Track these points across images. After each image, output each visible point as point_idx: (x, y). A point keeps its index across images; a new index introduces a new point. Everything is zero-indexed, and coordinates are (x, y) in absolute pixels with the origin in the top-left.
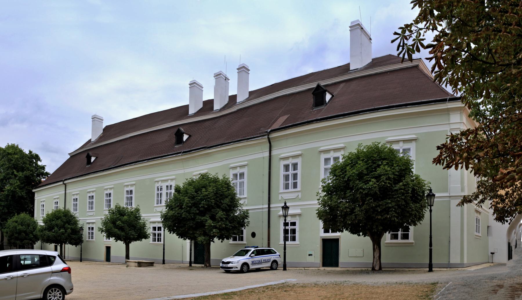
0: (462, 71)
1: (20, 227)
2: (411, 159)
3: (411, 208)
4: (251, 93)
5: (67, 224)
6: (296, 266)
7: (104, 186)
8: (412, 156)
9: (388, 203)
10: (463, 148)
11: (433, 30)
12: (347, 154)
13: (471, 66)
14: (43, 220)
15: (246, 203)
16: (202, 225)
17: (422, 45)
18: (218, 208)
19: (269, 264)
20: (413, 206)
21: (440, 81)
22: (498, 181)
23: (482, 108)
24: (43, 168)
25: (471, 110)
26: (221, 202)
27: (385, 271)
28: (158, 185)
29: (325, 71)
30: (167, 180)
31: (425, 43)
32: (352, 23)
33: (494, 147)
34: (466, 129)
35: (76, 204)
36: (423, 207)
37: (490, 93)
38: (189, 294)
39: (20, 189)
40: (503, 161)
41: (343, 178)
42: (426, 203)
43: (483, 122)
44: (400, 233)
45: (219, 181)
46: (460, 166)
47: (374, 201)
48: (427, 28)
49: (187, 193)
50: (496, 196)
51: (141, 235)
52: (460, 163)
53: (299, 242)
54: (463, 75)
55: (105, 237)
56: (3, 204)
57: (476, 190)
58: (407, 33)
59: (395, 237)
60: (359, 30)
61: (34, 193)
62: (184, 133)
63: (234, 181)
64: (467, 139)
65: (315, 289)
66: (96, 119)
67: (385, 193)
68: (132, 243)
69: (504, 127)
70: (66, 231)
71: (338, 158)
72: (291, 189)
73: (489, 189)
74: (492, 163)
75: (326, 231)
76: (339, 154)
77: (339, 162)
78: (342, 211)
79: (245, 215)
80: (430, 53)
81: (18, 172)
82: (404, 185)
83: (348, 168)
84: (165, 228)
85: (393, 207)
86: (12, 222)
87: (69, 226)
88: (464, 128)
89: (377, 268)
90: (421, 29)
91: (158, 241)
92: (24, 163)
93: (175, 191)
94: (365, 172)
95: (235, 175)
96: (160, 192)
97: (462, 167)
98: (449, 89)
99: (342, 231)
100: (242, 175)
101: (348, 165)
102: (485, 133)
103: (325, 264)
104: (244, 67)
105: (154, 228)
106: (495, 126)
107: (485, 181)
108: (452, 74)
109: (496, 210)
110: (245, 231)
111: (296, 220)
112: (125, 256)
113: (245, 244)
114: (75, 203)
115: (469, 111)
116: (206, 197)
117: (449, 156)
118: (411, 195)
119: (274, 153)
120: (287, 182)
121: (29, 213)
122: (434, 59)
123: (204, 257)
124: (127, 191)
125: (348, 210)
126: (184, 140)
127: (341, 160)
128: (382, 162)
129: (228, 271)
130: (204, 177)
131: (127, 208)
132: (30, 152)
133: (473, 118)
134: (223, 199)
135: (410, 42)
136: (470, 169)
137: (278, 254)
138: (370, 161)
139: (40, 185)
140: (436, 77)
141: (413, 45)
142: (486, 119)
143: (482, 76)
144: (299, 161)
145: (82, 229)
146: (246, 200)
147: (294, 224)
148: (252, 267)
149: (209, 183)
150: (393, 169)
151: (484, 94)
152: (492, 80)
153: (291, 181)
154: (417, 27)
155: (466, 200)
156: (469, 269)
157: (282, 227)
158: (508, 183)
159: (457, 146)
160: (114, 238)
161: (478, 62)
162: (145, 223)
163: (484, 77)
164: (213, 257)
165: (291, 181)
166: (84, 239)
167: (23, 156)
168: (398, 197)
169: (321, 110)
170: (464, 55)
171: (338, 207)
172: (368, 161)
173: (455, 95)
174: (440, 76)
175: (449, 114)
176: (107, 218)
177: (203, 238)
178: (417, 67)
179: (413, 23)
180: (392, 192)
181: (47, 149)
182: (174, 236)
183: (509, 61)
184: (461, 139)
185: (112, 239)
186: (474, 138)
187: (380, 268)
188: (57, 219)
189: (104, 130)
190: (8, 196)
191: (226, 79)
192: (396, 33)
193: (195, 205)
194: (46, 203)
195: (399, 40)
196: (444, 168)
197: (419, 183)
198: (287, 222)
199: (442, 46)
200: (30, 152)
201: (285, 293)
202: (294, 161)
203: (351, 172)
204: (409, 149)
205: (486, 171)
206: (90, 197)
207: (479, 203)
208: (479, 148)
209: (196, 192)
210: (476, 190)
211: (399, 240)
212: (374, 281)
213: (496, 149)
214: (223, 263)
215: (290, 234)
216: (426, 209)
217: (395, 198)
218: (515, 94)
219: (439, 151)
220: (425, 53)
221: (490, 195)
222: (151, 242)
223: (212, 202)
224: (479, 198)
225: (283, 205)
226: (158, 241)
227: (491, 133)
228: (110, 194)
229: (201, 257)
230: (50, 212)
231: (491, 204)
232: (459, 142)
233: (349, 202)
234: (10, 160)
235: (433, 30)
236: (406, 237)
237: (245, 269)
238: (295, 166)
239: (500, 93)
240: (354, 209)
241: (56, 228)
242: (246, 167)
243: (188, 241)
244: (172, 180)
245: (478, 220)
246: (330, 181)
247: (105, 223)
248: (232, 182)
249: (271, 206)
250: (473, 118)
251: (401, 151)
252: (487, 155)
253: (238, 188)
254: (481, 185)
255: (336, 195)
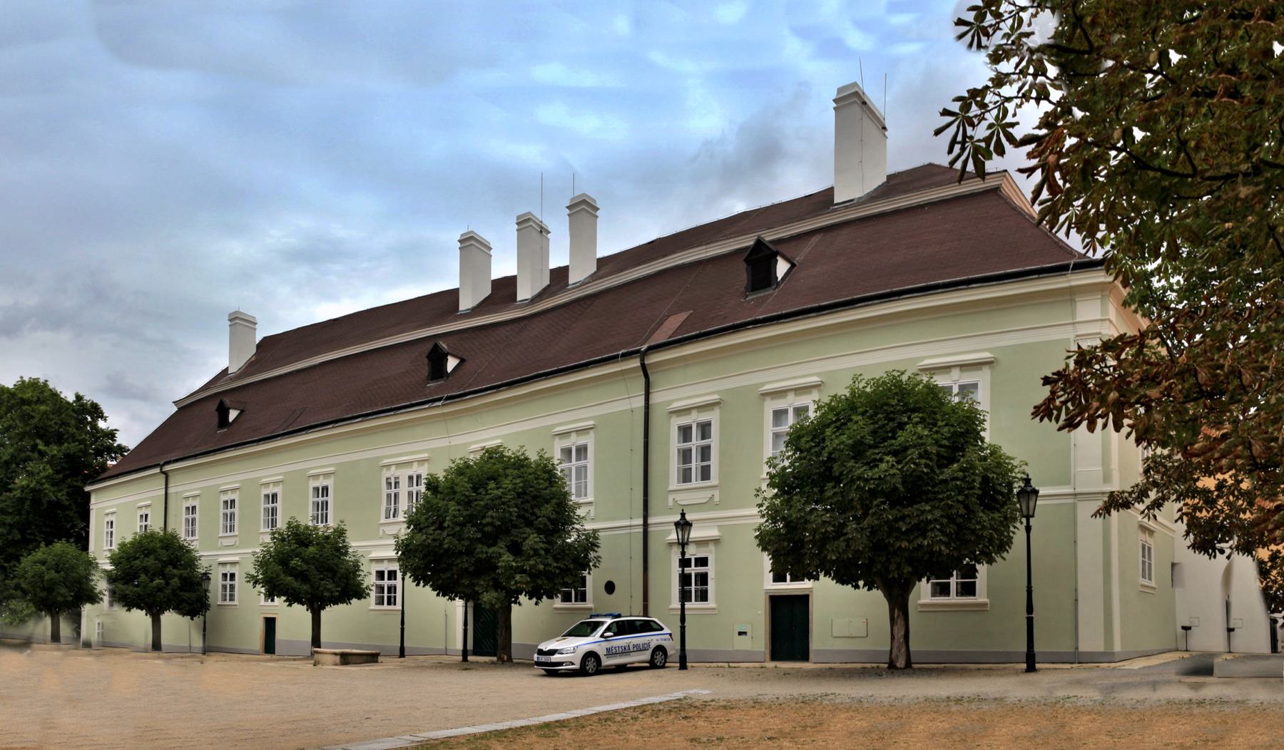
0: (1109, 197)
1: (53, 574)
2: (980, 408)
3: (979, 523)
4: (602, 262)
5: (170, 567)
6: (708, 658)
7: (260, 478)
8: (983, 400)
9: (924, 512)
10: (1108, 379)
11: (1038, 100)
12: (826, 400)
13: (1133, 185)
14: (111, 558)
15: (592, 514)
16: (487, 566)
17: (1011, 139)
18: (527, 526)
19: (646, 656)
20: (985, 518)
21: (1053, 224)
22: (1197, 455)
23: (1156, 283)
24: (111, 435)
25: (1128, 289)
26: (534, 514)
27: (919, 669)
28: (388, 475)
29: (773, 206)
30: (409, 464)
31: (1018, 133)
32: (840, 90)
33: (1187, 376)
34: (1116, 335)
35: (193, 520)
36: (1008, 520)
37: (1178, 248)
38: (462, 726)
39: (52, 485)
40: (1211, 409)
41: (818, 454)
42: (1017, 510)
43: (1159, 316)
44: (953, 581)
45: (529, 466)
46: (1100, 422)
47: (892, 506)
48: (1024, 96)
49: (455, 493)
50: (1194, 492)
51: (349, 589)
52: (1100, 416)
53: (717, 602)
54: (1111, 207)
55: (262, 596)
56: (9, 520)
57: (1140, 479)
58: (975, 110)
59: (943, 590)
60: (857, 109)
61: (88, 495)
62: (448, 354)
63: (564, 465)
64: (1117, 358)
65: (756, 712)
66: (240, 322)
67: (916, 489)
68: (328, 608)
69: (1213, 328)
70: (167, 584)
71: (806, 409)
72: (696, 482)
73: (1175, 476)
74: (1180, 413)
75: (779, 578)
76: (807, 400)
77: (807, 417)
78: (814, 532)
79: (590, 542)
80: (1030, 155)
81: (47, 444)
82: (962, 470)
83: (828, 432)
84: (404, 574)
85: (936, 520)
86: (32, 562)
87: (175, 571)
88: (1112, 333)
89: (900, 662)
90: (1009, 99)
91: (389, 603)
92: (64, 424)
93: (428, 489)
94: (869, 440)
95: (567, 452)
96: (393, 491)
97: (1105, 426)
98: (1075, 241)
99: (817, 578)
100: (582, 451)
101: (828, 426)
102: (1163, 343)
103: (777, 653)
104: (584, 202)
105: (380, 575)
106: (1191, 325)
107: (1165, 457)
108: (1084, 206)
109: (1193, 525)
110: (589, 580)
111: (709, 552)
112: (310, 639)
113: (590, 609)
114: (190, 516)
115: (1125, 292)
116: (497, 502)
117: (1072, 400)
118: (980, 492)
119: (656, 398)
120: (687, 466)
121: (76, 542)
122: (1039, 171)
123: (495, 640)
124: (316, 489)
125: (830, 529)
126: (449, 370)
127: (812, 415)
128: (909, 418)
129: (553, 671)
130: (492, 455)
131: (316, 528)
132: (79, 398)
133: (1133, 307)
134: (538, 506)
135: (981, 132)
136: (1126, 430)
137: (666, 630)
138: (880, 416)
139: (103, 476)
140: (1043, 214)
141: (987, 140)
142: (1168, 309)
143: (1160, 207)
144: (713, 417)
145: (206, 577)
146: (592, 509)
147: (703, 562)
148: (606, 662)
149: (505, 469)
150: (937, 432)
151: (1163, 249)
152: (1186, 216)
153: (695, 464)
154: (999, 95)
155: (1116, 502)
156: (1127, 665)
157: (676, 570)
158: (1224, 462)
159: (1093, 375)
160: (284, 598)
161: (1151, 174)
162: (357, 561)
163: (1163, 209)
164: (517, 637)
165: (696, 464)
166: (211, 601)
167: (60, 408)
168: (949, 497)
169: (765, 298)
170: (1115, 158)
171: (806, 522)
172: (876, 414)
173: (1090, 254)
174: (1052, 212)
175: (1073, 301)
176: (268, 551)
177: (495, 594)
178: (996, 190)
179: (990, 84)
180: (934, 486)
181: (120, 390)
182: (427, 592)
183: (1231, 166)
184: (1103, 360)
185: (279, 601)
186: (1135, 356)
187: (909, 664)
188: (146, 556)
189: (259, 346)
190: (21, 501)
191: (543, 231)
192: (946, 113)
193: (471, 519)
194: (118, 516)
195: (953, 128)
196: (1060, 429)
197: (998, 463)
198: (687, 556)
199: (1060, 140)
200: (79, 398)
201: (685, 722)
202: (703, 417)
203: (836, 441)
204: (975, 386)
205: (1165, 433)
206: (226, 502)
207: (1148, 508)
208: (1148, 379)
209: (475, 489)
210: (1140, 479)
211: (953, 599)
212: (895, 695)
213: (1192, 380)
214: (541, 652)
215: (694, 585)
216: (1018, 524)
217: (942, 500)
218: (1244, 247)
219: (1048, 388)
220: (1016, 158)
221: (1176, 491)
222: (373, 606)
223: (511, 513)
224: (1148, 496)
225: (678, 518)
226: (389, 603)
227: (1180, 342)
228: (274, 496)
229: (490, 641)
230: (129, 539)
231: (1180, 510)
232: (1097, 367)
233: (832, 510)
234: (26, 418)
235: (1038, 100)
236: (968, 589)
237: (591, 666)
238: (705, 429)
239: (1206, 246)
240: (843, 525)
241: (143, 577)
242: (592, 432)
243: (459, 603)
244: (421, 462)
245: (1146, 550)
246: (787, 463)
247: (263, 564)
248: (559, 468)
249: (650, 521)
250: (1133, 307)
251: (956, 390)
252: (1169, 396)
253: (574, 481)
254: (1152, 465)
255: (802, 493)
